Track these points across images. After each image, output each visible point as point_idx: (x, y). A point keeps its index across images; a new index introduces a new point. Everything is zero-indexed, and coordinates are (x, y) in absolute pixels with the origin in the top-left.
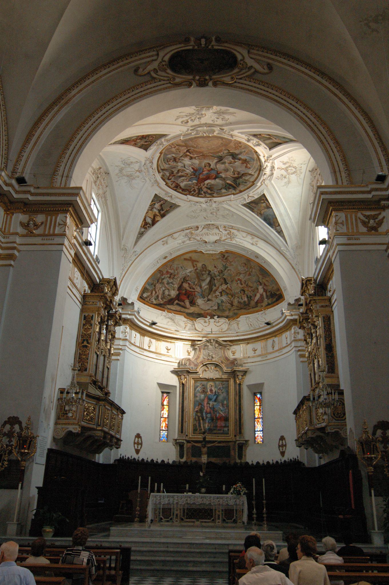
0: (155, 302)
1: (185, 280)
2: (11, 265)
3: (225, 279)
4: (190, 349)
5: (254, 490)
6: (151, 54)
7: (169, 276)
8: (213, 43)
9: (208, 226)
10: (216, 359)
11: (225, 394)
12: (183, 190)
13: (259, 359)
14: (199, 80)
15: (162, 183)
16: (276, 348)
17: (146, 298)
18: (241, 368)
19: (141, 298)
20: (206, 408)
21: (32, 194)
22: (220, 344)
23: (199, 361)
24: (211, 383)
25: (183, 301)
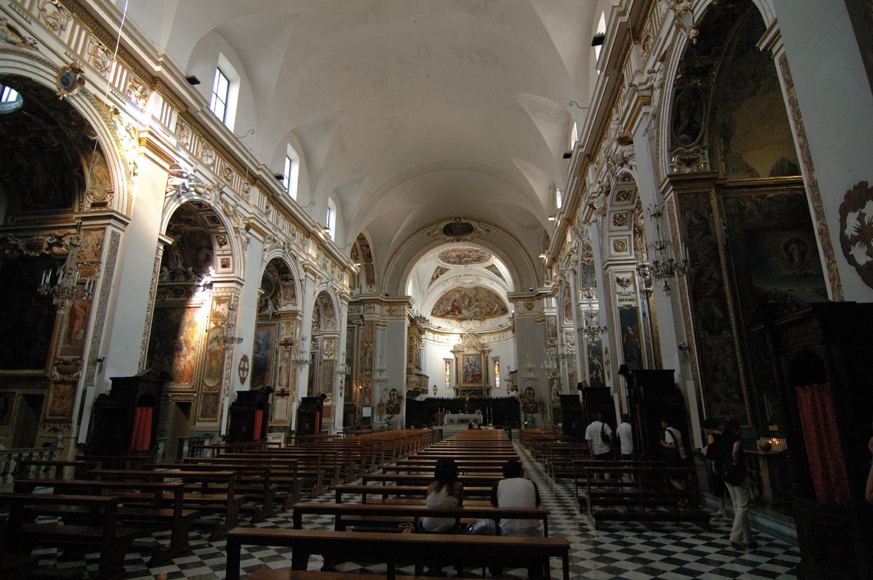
0: (439, 314)
1: (455, 301)
3: (477, 300)
4: (460, 338)
9: (466, 275)
10: (474, 344)
11: (479, 362)
13: (497, 343)
15: (441, 262)
16: (505, 338)
18: (487, 349)
19: (432, 314)
20: (470, 370)
22: (476, 335)
23: (465, 345)
24: (472, 357)
25: (455, 312)
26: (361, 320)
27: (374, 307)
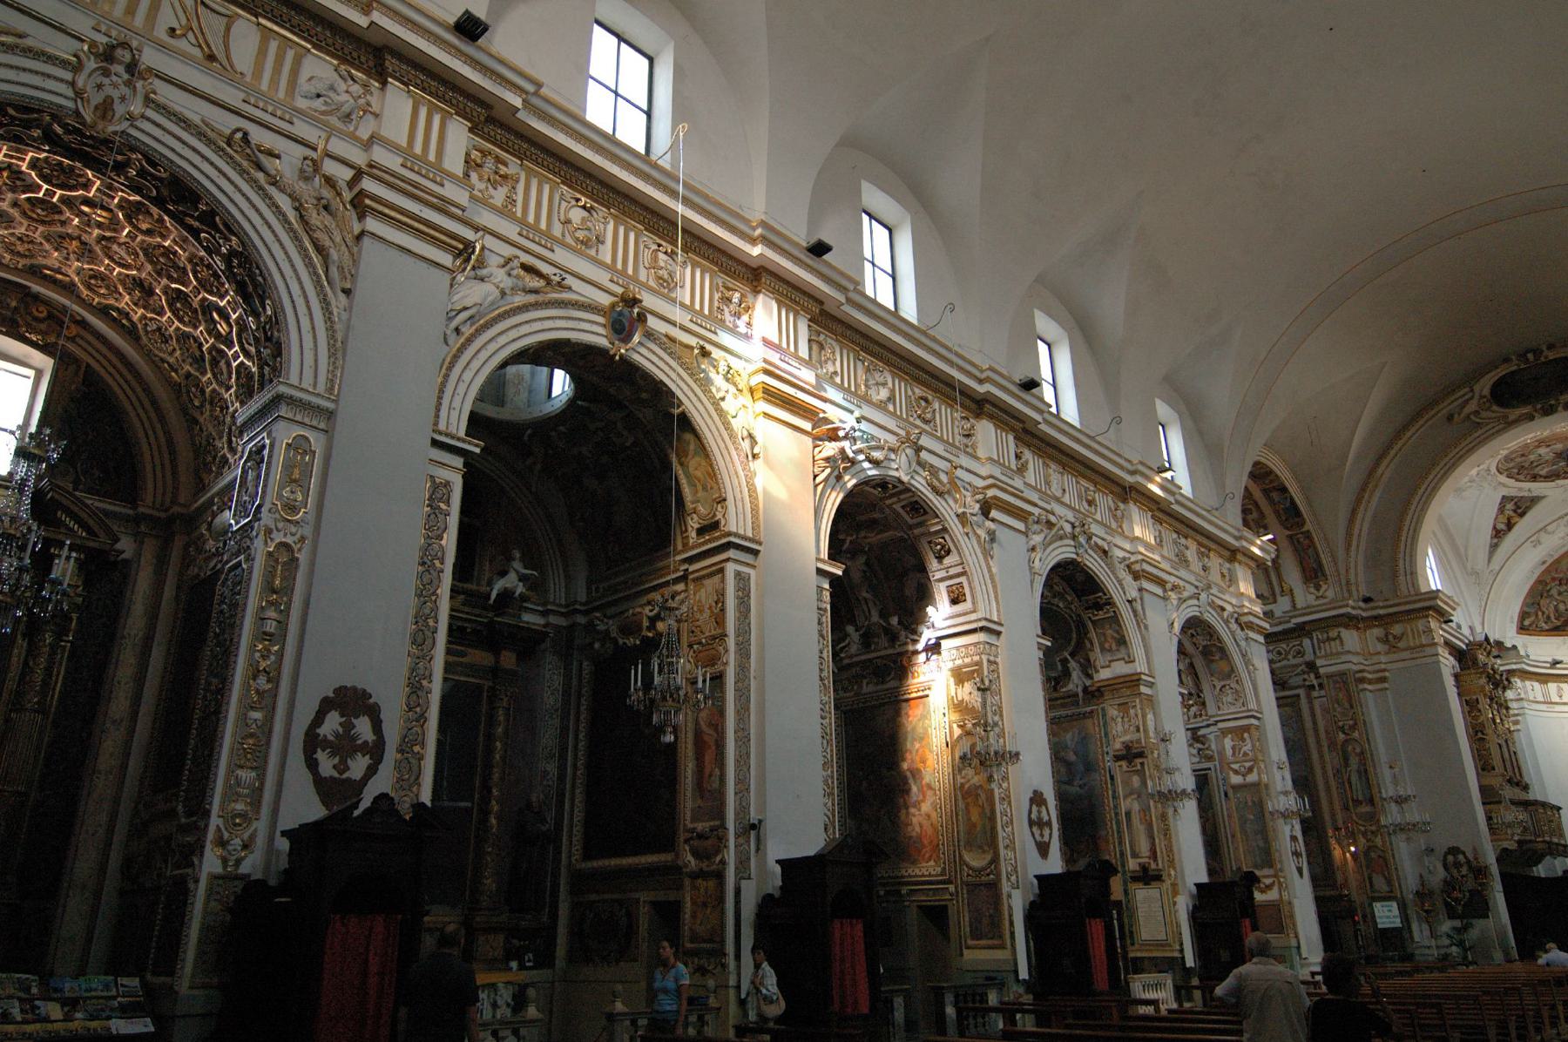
0: (1546, 627)
2: (1386, 689)
5: (606, 862)
6: (1462, 393)
7: (1557, 582)
8: (1546, 352)
12: (1545, 477)
14: (1542, 408)
15: (1511, 482)
17: (1530, 625)
19: (1522, 629)
21: (1382, 608)
26: (1312, 676)
27: (1339, 636)
